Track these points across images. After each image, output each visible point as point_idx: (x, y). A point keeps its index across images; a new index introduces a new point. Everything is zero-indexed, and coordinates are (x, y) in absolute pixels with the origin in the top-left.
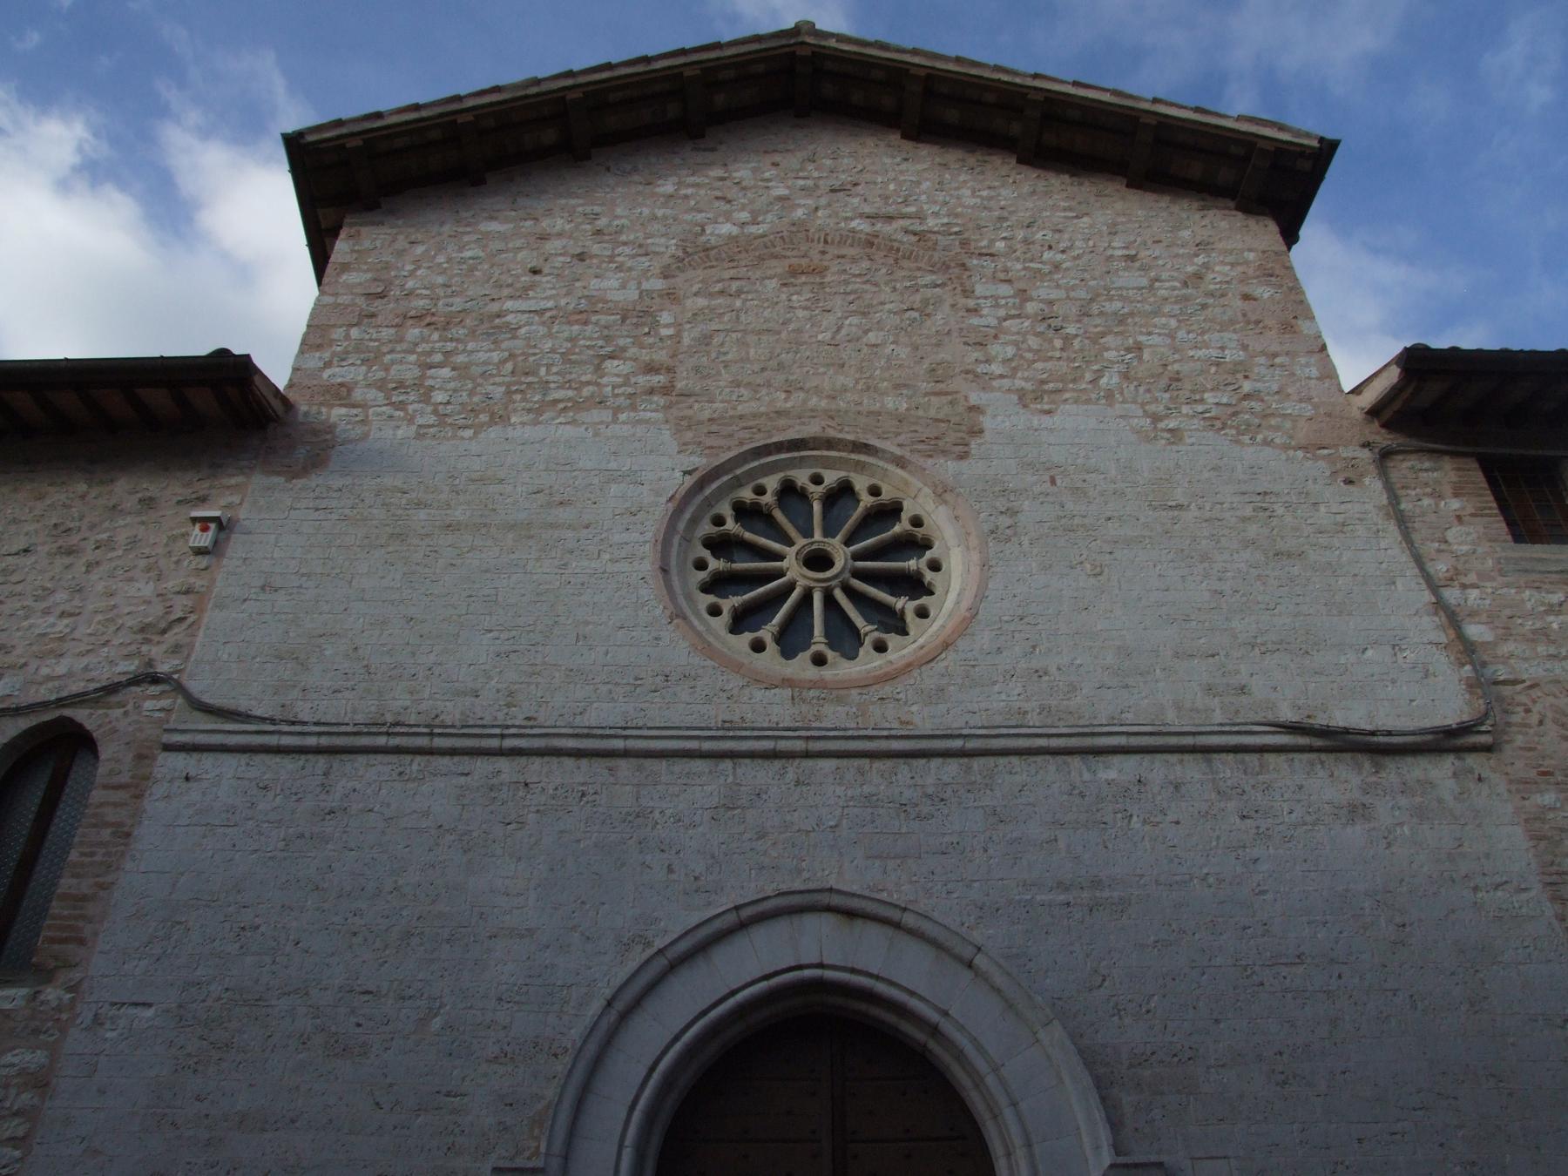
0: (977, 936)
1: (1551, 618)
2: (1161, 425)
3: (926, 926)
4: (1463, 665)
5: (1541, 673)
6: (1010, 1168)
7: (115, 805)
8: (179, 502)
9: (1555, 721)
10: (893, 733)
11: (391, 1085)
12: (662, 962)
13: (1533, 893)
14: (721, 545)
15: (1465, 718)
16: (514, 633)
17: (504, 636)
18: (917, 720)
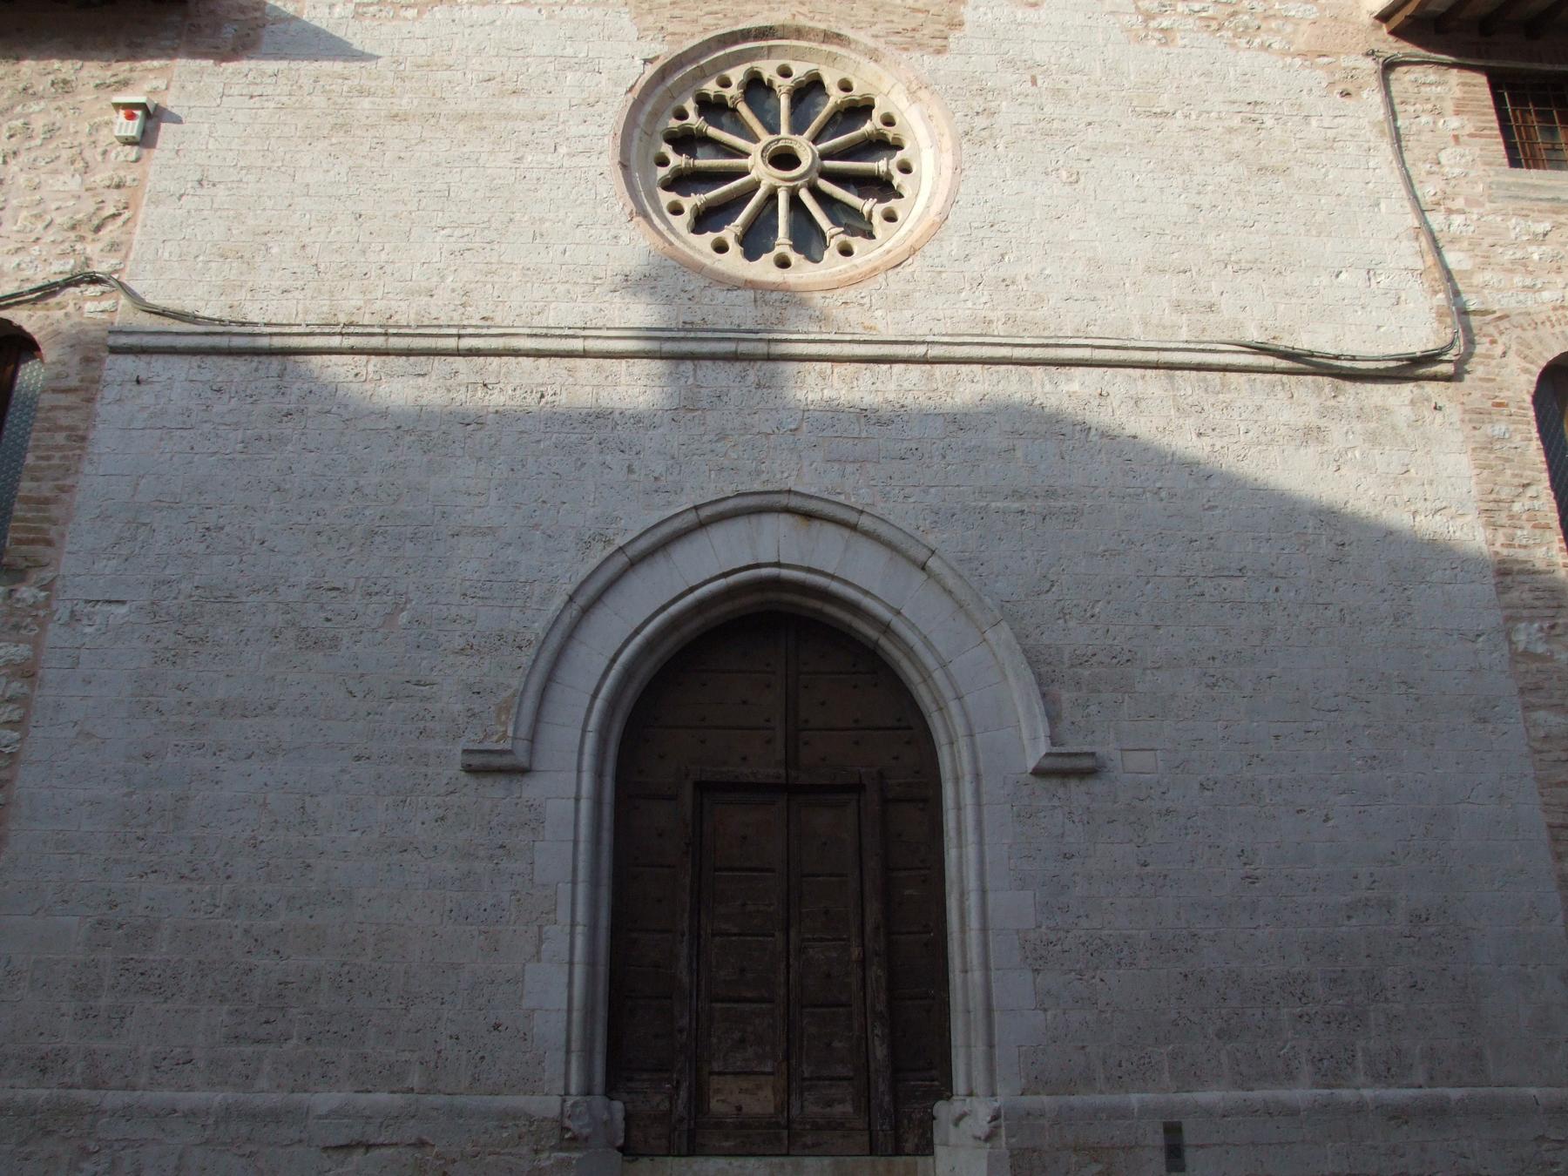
0: (931, 540)
1: (1531, 249)
2: (1153, 24)
3: (883, 530)
4: (1436, 293)
5: (1513, 304)
6: (952, 755)
7: (68, 409)
8: (97, 86)
9: (1519, 353)
10: (856, 337)
11: (362, 675)
12: (622, 560)
13: (1469, 518)
14: (685, 141)
15: (1430, 347)
16: (467, 231)
17: (458, 233)
18: (880, 326)
